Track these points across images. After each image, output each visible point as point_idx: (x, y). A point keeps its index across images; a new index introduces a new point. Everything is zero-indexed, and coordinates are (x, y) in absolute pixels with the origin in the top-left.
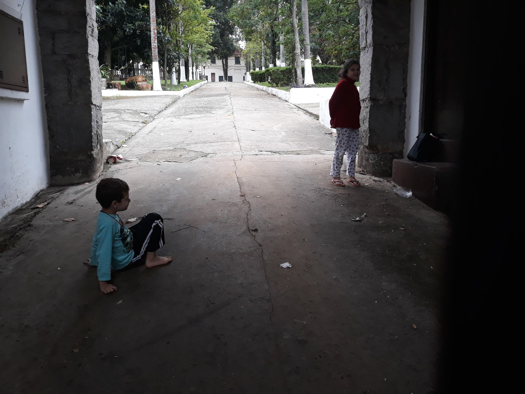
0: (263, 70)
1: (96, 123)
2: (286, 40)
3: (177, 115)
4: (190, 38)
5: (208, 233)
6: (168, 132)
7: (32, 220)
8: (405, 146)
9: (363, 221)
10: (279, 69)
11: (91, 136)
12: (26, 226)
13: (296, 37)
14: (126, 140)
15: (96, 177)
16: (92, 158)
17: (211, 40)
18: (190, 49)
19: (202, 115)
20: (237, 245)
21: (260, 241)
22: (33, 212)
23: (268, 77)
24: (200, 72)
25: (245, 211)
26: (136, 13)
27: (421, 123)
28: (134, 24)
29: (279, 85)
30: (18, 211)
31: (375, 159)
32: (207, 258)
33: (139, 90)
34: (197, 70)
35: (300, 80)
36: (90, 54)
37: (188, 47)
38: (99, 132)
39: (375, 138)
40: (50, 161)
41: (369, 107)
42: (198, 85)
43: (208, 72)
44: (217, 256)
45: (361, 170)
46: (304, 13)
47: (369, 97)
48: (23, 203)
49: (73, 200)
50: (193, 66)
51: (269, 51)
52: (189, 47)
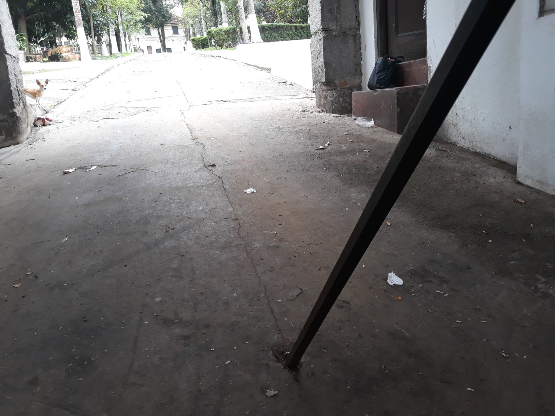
1: (14, 76)
5: (160, 173)
8: (363, 79)
9: (326, 149)
10: (221, 29)
11: (11, 92)
14: (55, 105)
15: (24, 139)
18: (119, 17)
20: (194, 179)
21: (219, 175)
23: (211, 40)
24: (134, 46)
27: (377, 51)
29: (224, 47)
31: (333, 95)
37: (116, 14)
38: (19, 87)
39: (331, 72)
44: (172, 191)
45: (320, 110)
47: (321, 28)
50: (125, 37)
52: (118, 15)
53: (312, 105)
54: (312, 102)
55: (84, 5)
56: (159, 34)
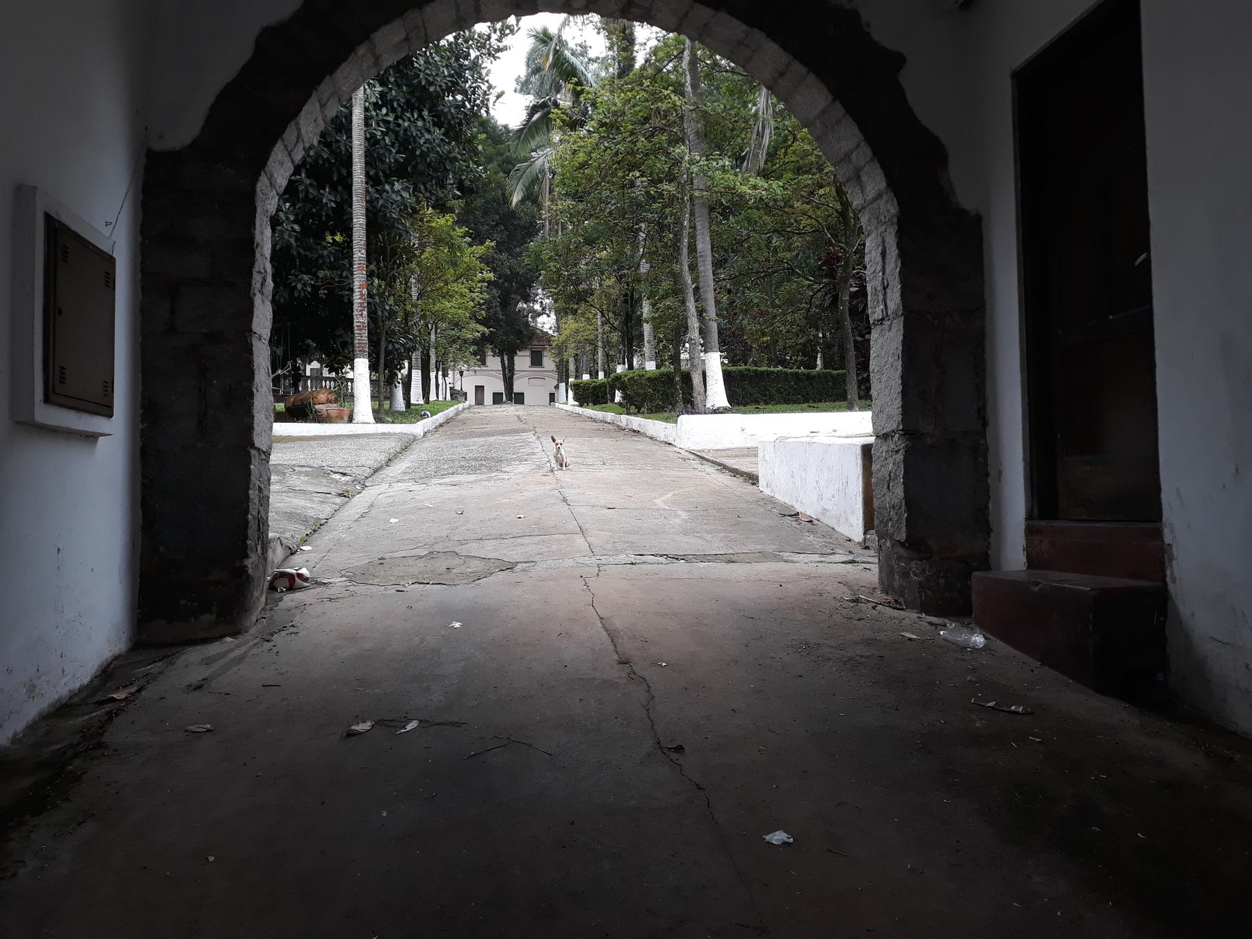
0: (600, 378)
1: (257, 492)
2: (662, 311)
3: (421, 476)
4: (438, 306)
6: (407, 515)
7: (105, 731)
8: (991, 540)
10: (643, 375)
11: (247, 522)
12: (91, 747)
13: (688, 304)
14: (307, 535)
16: (245, 577)
17: (483, 312)
19: (480, 477)
22: (103, 710)
25: (638, 700)
26: (320, 252)
28: (315, 275)
30: (63, 709)
31: (923, 571)
32: (572, 823)
33: (319, 423)
34: (446, 378)
35: (698, 398)
36: (255, 333)
38: (262, 513)
40: (140, 584)
41: (901, 452)
42: (451, 411)
43: (468, 384)
45: (890, 598)
46: (703, 254)
48: (74, 690)
49: (203, 680)
51: (615, 337)
52: (432, 328)
53: (870, 583)
54: (869, 572)
55: (375, 312)
56: (503, 365)
